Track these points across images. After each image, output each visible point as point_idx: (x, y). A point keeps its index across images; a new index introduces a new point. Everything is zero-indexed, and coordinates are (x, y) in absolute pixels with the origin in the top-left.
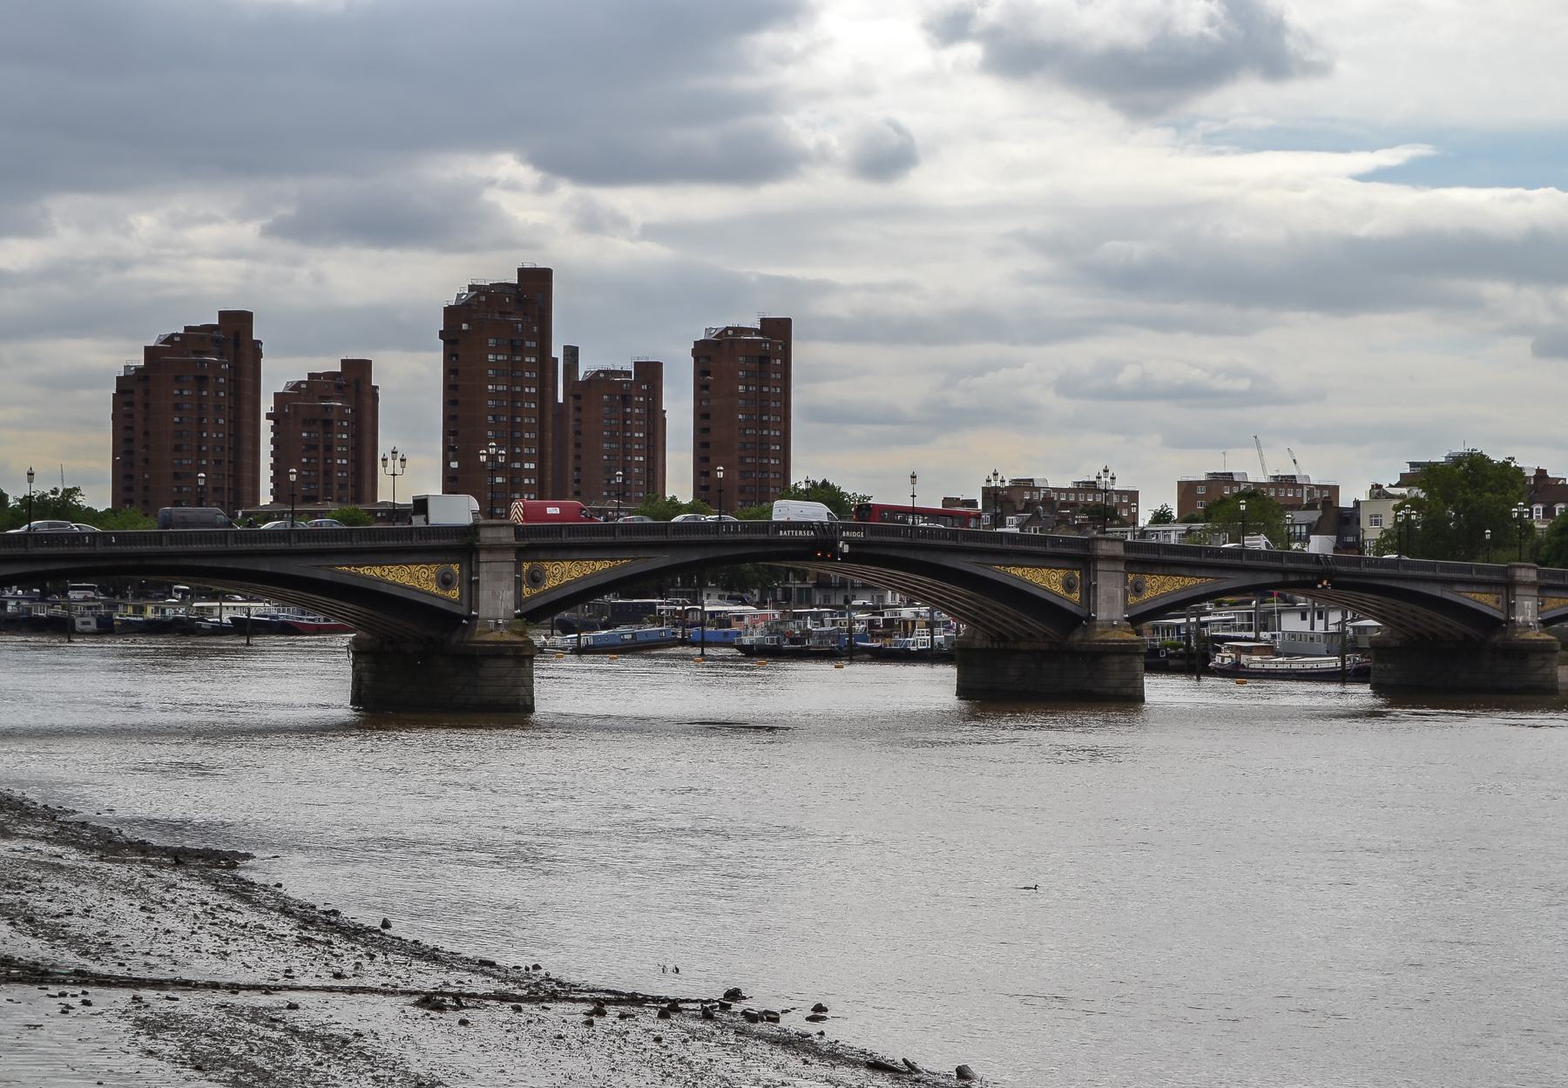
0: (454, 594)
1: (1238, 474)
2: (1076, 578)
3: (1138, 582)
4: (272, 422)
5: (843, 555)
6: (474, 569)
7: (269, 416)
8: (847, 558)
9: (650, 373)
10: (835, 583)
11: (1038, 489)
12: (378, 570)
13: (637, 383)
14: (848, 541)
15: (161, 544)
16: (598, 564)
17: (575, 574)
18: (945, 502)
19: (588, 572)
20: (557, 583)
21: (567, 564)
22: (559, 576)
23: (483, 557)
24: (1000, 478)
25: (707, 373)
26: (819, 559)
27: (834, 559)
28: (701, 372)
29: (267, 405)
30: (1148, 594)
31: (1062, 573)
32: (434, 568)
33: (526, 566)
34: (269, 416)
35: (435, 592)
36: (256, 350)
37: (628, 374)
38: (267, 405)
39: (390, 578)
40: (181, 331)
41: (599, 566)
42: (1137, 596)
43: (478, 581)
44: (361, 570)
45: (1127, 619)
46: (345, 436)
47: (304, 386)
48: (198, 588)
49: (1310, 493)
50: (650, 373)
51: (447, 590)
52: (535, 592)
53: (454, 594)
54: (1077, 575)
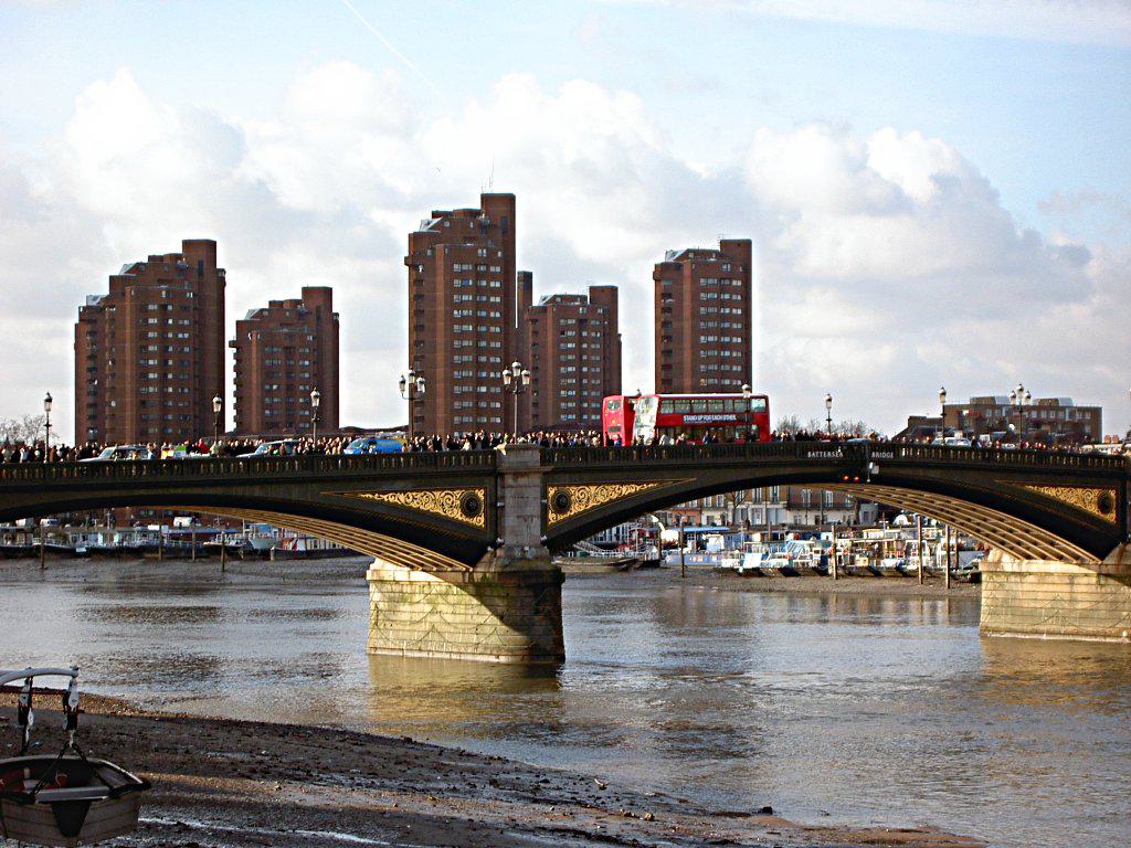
0: (479, 521)
1: (1062, 399)
2: (479, 499)
3: (560, 497)
4: (235, 350)
5: (872, 476)
6: (499, 493)
7: (232, 344)
8: (877, 480)
9: (605, 298)
10: (807, 504)
11: (1000, 407)
12: (402, 497)
13: (592, 310)
14: (878, 462)
15: (745, 455)
16: (624, 489)
17: (601, 499)
18: (912, 421)
19: (614, 496)
20: (583, 508)
21: (593, 489)
22: (585, 500)
23: (509, 480)
24: (1026, 395)
25: (670, 296)
26: (847, 482)
27: (862, 481)
28: (662, 295)
29: (230, 333)
30: (576, 509)
31: (1096, 492)
32: (458, 493)
33: (552, 492)
34: (232, 344)
35: (460, 518)
36: (220, 280)
37: (583, 298)
38: (230, 333)
39: (415, 505)
40: (146, 260)
41: (626, 490)
42: (1103, 512)
43: (503, 507)
44: (385, 497)
45: (543, 543)
46: (307, 363)
47: (266, 313)
48: (227, 520)
49: (1072, 414)
50: (605, 298)
51: (472, 516)
52: (561, 517)
53: (479, 521)
54: (1112, 494)
